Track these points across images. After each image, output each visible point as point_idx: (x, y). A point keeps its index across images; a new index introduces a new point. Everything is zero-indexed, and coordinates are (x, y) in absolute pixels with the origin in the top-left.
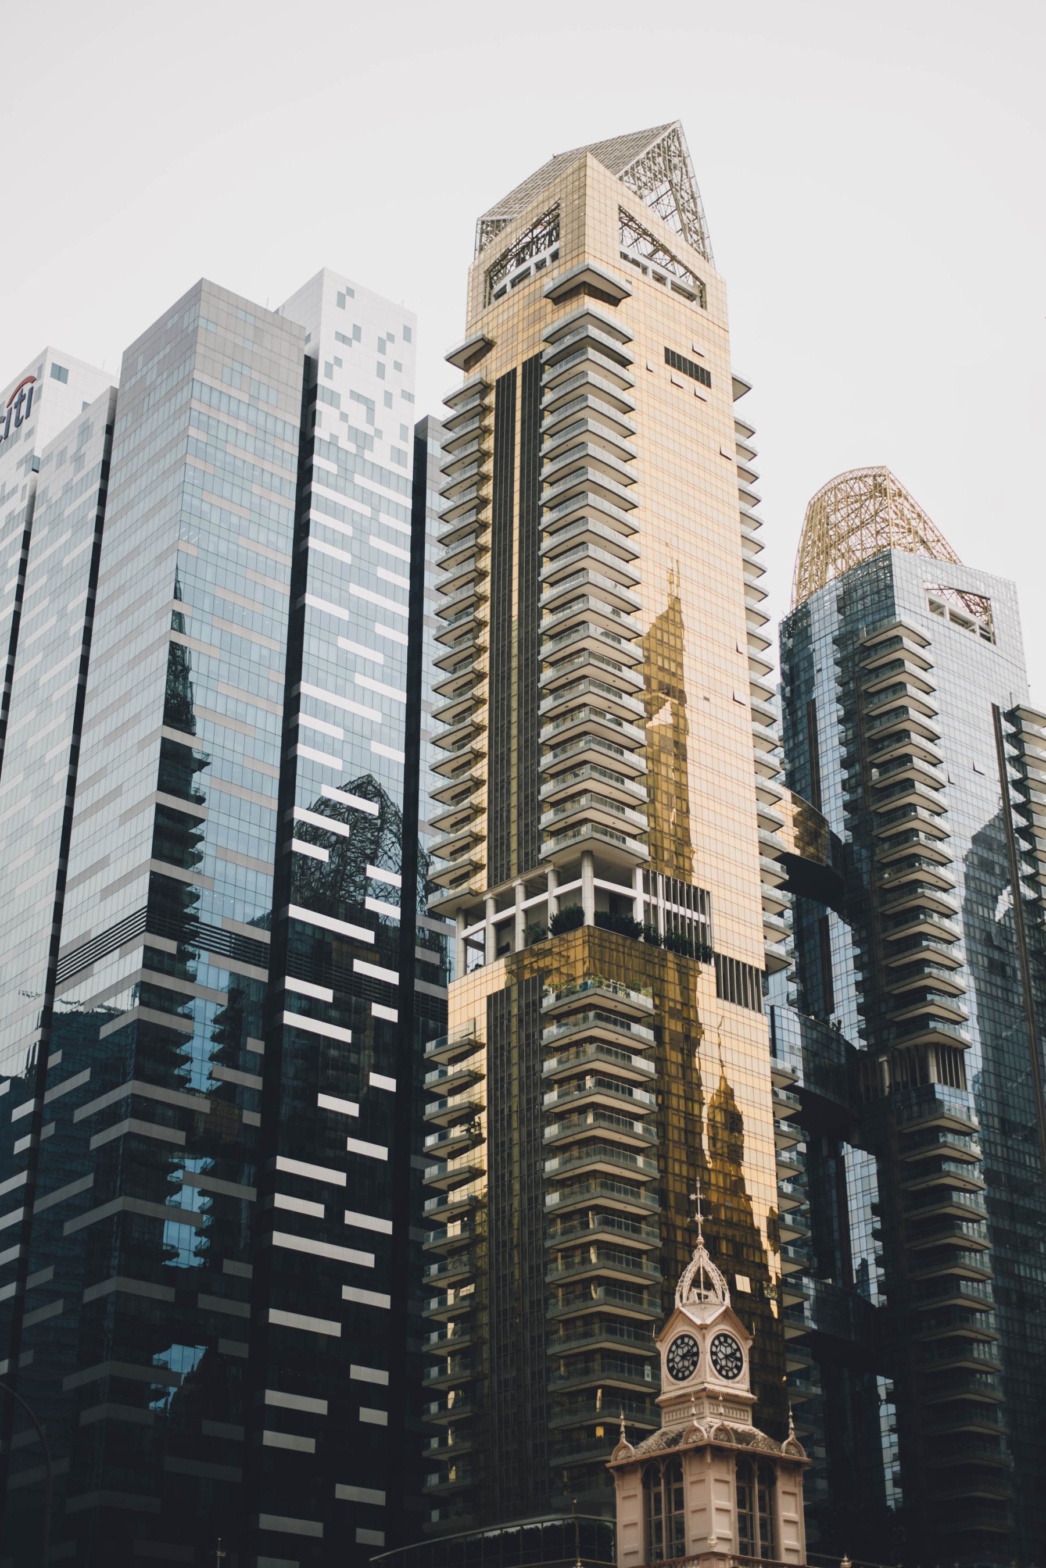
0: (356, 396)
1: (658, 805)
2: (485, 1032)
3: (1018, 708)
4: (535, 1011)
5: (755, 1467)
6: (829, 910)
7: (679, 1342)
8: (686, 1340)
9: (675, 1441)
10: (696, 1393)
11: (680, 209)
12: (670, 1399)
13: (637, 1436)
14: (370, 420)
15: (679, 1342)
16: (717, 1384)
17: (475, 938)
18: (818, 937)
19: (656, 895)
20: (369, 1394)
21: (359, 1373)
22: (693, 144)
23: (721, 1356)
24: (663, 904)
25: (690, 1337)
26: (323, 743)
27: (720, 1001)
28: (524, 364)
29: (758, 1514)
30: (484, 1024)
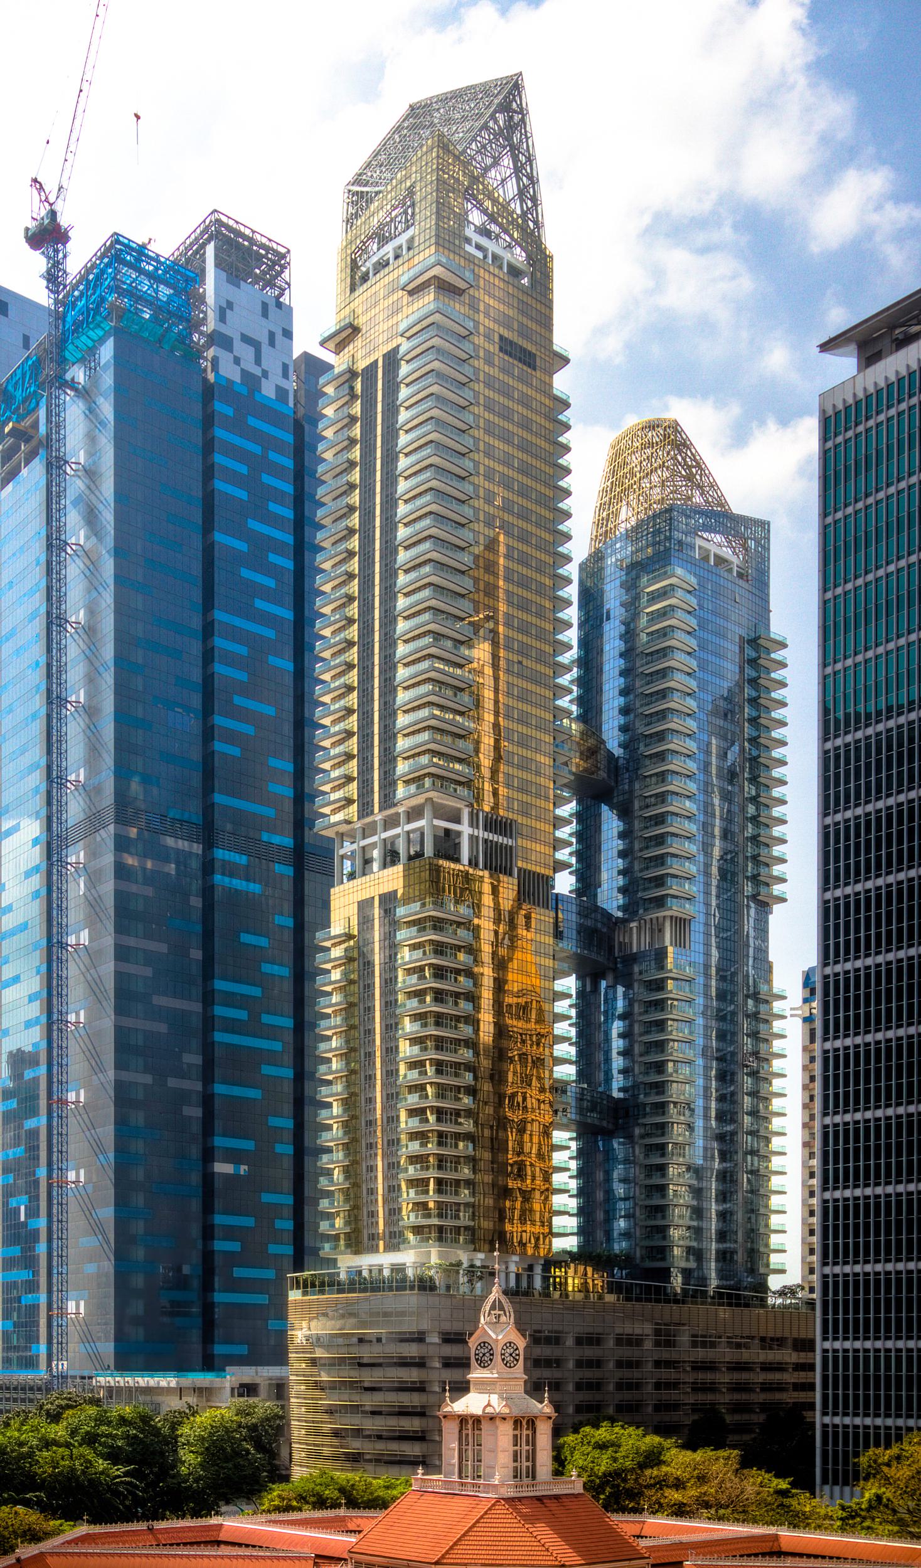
0: (246, 339)
1: (481, 756)
3: (759, 637)
11: (518, 170)
14: (258, 361)
19: (478, 828)
22: (533, 98)
24: (482, 834)
26: (232, 660)
28: (384, 356)
30: (356, 922)
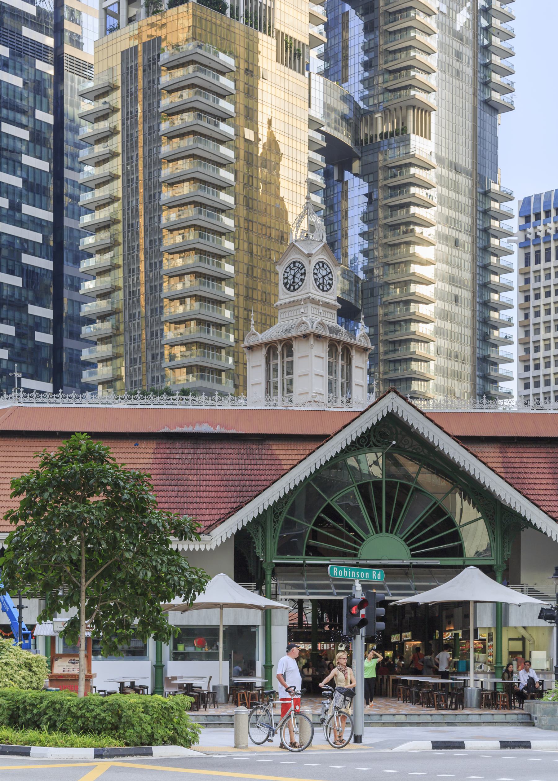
2: (119, 78)
4: (154, 64)
5: (340, 349)
6: (348, 7)
7: (292, 266)
8: (297, 264)
9: (288, 331)
10: (304, 299)
12: (285, 304)
13: (264, 326)
15: (292, 266)
16: (317, 294)
17: (111, 8)
18: (340, 26)
20: (39, 324)
21: (34, 310)
23: (320, 276)
25: (300, 263)
27: (278, 65)
29: (340, 380)
30: (119, 72)
